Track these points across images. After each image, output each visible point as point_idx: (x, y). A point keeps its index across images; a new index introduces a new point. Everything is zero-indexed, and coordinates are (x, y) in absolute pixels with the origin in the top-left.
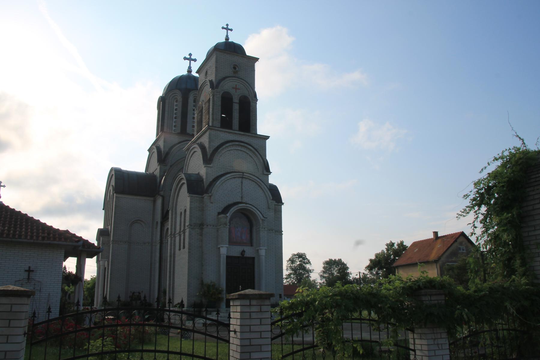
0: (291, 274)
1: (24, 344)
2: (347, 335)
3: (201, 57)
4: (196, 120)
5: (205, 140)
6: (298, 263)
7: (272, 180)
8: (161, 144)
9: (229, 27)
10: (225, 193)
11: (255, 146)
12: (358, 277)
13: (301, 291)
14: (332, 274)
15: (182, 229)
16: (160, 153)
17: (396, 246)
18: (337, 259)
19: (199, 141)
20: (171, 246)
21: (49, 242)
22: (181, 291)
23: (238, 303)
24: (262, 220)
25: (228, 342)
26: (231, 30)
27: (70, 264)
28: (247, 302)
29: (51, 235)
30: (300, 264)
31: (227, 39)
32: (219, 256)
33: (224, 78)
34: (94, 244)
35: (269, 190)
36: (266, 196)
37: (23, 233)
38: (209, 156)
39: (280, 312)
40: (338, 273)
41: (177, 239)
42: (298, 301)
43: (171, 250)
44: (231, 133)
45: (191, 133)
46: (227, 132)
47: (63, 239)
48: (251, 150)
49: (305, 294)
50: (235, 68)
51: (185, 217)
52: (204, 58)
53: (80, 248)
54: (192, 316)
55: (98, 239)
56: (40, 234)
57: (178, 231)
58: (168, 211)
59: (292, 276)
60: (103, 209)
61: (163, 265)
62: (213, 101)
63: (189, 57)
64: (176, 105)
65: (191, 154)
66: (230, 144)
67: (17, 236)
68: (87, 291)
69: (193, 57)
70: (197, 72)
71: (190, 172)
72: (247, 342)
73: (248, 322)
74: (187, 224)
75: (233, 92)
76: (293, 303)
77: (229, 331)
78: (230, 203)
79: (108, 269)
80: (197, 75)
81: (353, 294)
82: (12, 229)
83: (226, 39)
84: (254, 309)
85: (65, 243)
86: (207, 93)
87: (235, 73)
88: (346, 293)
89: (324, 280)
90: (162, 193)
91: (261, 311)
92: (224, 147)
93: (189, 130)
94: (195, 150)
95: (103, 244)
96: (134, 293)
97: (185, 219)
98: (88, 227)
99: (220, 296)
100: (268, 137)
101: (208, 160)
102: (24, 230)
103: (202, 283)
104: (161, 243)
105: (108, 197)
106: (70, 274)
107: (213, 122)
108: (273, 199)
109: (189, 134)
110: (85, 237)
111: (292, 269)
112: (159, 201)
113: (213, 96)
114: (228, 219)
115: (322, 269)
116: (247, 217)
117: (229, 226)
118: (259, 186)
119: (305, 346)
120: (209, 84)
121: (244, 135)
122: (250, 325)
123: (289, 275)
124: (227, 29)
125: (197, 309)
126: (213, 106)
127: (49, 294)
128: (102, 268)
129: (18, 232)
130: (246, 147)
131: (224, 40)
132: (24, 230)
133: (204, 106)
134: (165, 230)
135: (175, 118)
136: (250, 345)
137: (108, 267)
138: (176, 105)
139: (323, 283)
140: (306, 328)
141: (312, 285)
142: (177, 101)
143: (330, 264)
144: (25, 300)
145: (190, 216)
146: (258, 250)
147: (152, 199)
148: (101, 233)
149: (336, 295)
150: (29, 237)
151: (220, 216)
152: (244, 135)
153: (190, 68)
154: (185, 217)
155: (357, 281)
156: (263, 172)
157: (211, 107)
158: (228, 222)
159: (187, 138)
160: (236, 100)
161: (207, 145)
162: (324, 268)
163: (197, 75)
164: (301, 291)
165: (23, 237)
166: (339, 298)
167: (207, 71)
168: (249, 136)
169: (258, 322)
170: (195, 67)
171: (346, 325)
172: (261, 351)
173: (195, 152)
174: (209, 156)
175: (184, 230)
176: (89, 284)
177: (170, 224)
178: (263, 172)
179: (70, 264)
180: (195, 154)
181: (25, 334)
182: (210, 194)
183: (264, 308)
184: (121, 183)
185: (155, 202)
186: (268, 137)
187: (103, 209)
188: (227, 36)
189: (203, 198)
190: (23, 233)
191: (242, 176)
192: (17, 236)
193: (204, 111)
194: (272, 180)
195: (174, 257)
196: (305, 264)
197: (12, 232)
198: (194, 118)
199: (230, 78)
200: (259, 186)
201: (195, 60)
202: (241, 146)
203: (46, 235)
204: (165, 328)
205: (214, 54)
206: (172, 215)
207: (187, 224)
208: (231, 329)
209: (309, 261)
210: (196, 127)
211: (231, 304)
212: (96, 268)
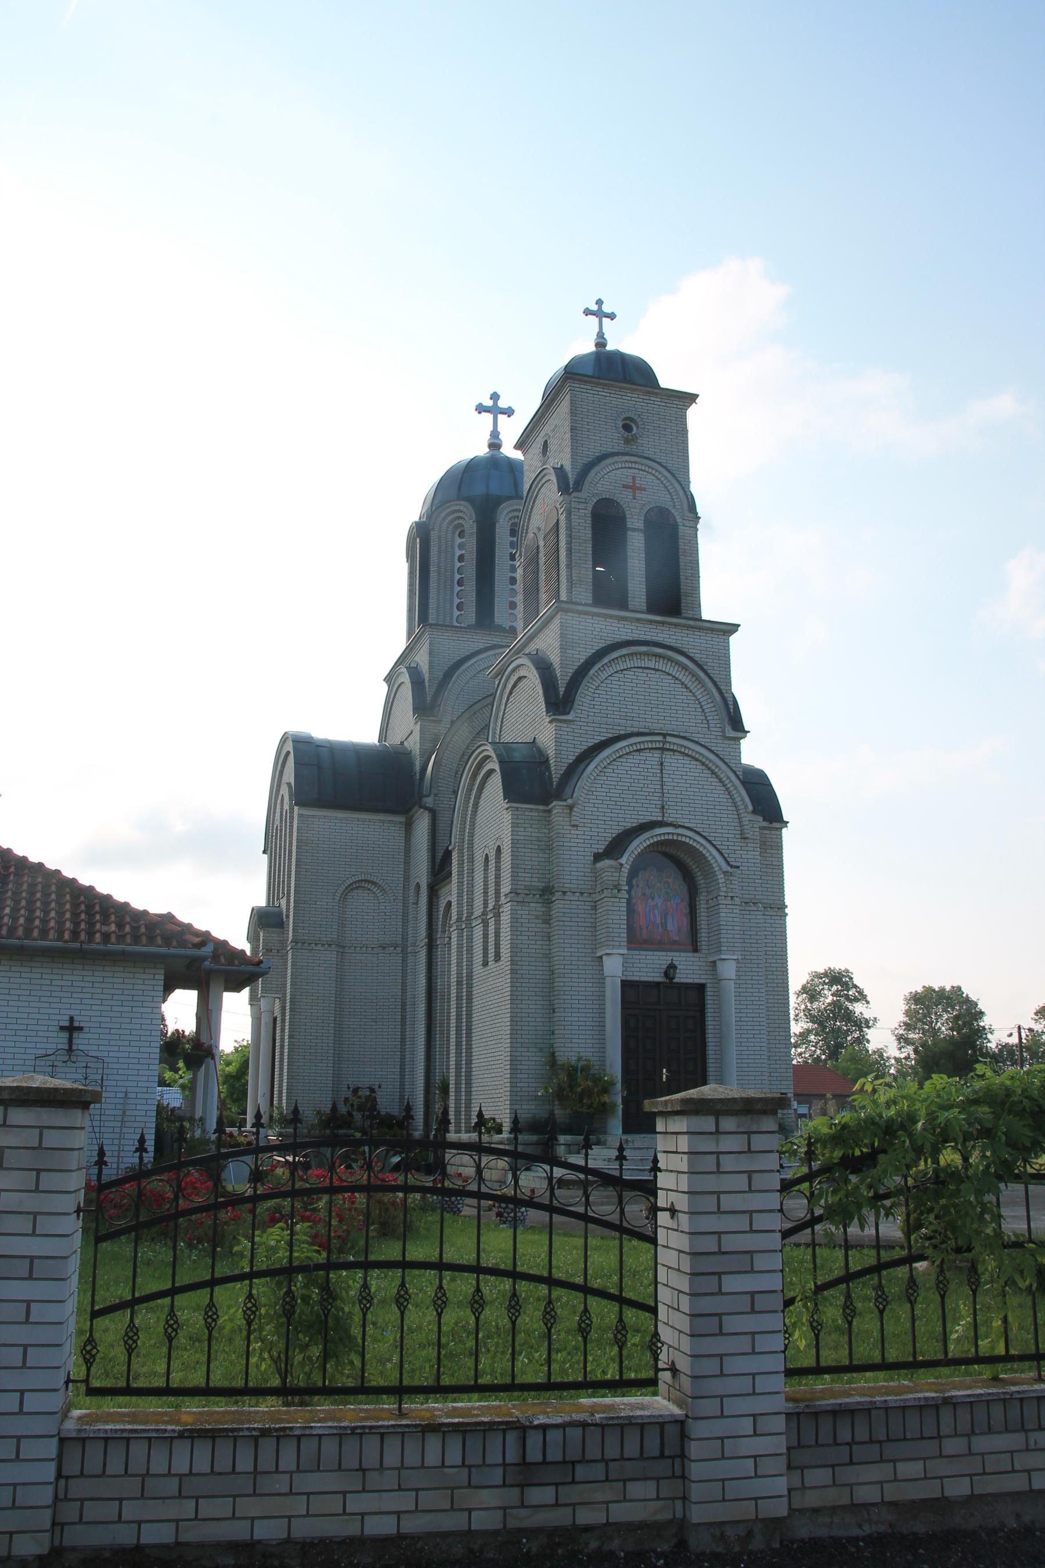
0: (808, 1032)
1: (78, 1236)
2: (1013, 1224)
3: (526, 403)
4: (519, 587)
5: (549, 643)
6: (830, 999)
7: (752, 753)
8: (422, 658)
9: (606, 309)
10: (607, 800)
11: (695, 653)
12: (1014, 1040)
13: (869, 1088)
14: (935, 1032)
15: (491, 905)
16: (419, 684)
18: (948, 988)
19: (531, 648)
20: (460, 953)
21: (121, 947)
22: (493, 1085)
23: (680, 1124)
24: (725, 873)
25: (653, 1241)
26: (612, 316)
27: (180, 1011)
28: (707, 1123)
29: (128, 929)
30: (833, 1003)
31: (601, 343)
33: (600, 459)
34: (243, 952)
35: (744, 783)
36: (734, 803)
37: (52, 924)
39: (806, 1153)
40: (951, 1029)
41: (478, 932)
42: (859, 1119)
43: (459, 965)
44: (625, 619)
45: (507, 625)
46: (612, 617)
47: (159, 940)
48: (685, 668)
49: (882, 1099)
50: (627, 428)
51: (498, 869)
52: (536, 403)
53: (204, 965)
54: (519, 1159)
55: (252, 937)
56: (98, 926)
57: (478, 911)
58: (448, 854)
59: (812, 1037)
60: (264, 852)
61: (437, 1013)
62: (569, 528)
63: (490, 403)
64: (461, 546)
65: (509, 686)
66: (624, 651)
67: (36, 933)
68: (224, 1083)
69: (502, 404)
70: (520, 445)
71: (507, 738)
72: (709, 1244)
73: (711, 1183)
74: (505, 889)
75: (624, 498)
76: (844, 1127)
77: (654, 1209)
78: (629, 825)
79: (283, 1021)
80: (518, 455)
81: (1030, 1098)
82: (22, 912)
83: (597, 345)
84: (728, 1143)
85: (164, 950)
86: (547, 505)
87: (627, 441)
88: (1008, 1095)
89: (909, 1050)
90: (429, 801)
91: (750, 1151)
92: (606, 660)
93: (500, 617)
94: (522, 672)
95: (268, 950)
96: (356, 1090)
97: (498, 877)
98: (223, 904)
99: (606, 1099)
100: (733, 628)
101: (559, 701)
102: (53, 914)
103: (552, 1062)
104: (431, 946)
105: (277, 817)
106: (178, 1035)
107: (570, 591)
108: (754, 812)
109: (500, 629)
110: (219, 934)
111: (812, 1018)
112: (422, 824)
113: (569, 513)
114: (625, 870)
115: (903, 1018)
116: (680, 862)
117: (629, 892)
118: (713, 773)
119: (886, 1256)
120: (554, 478)
121: (663, 623)
122: (719, 1193)
123: (804, 1035)
124: (599, 313)
125: (536, 1139)
126: (569, 543)
127: (126, 1093)
128: (265, 1019)
129: (37, 922)
130: (670, 659)
131: (592, 348)
132: (53, 914)
133: (541, 543)
134: (442, 909)
135: (460, 583)
136: (721, 1253)
137: (283, 1014)
138: (461, 546)
139: (907, 1058)
140: (887, 1203)
141: (875, 1065)
142: (461, 535)
143: (926, 1003)
144: (77, 1117)
145: (515, 867)
146: (714, 962)
147: (401, 819)
148: (264, 921)
149: (976, 1102)
150: (67, 936)
151: (600, 865)
152: (663, 623)
153: (495, 434)
154: (498, 869)
155: (1007, 1054)
157: (563, 544)
158: (624, 880)
159: (496, 641)
160: (635, 521)
161: (555, 658)
162: (907, 1013)
163: (518, 455)
164: (869, 1088)
165: (52, 934)
166: (987, 1109)
167: (546, 442)
168: (676, 625)
169: (742, 1183)
170: (511, 431)
171: (1011, 1191)
172: (752, 1271)
173: (520, 679)
174: (562, 690)
175: (497, 907)
176: (228, 1064)
177: (455, 891)
178: (723, 731)
179: (180, 1011)
180: (521, 685)
181: (78, 1211)
182: (570, 801)
183: (759, 1142)
184: (318, 780)
185: (409, 826)
186: (733, 628)
187: (264, 852)
188: (601, 335)
189: (550, 811)
190: (52, 924)
191: (664, 742)
192: (36, 933)
193: (542, 559)
194: (752, 753)
195: (470, 986)
196: (851, 1001)
197: (22, 921)
198: (513, 581)
199: (616, 459)
200: (713, 773)
201: (509, 412)
202: (656, 655)
203: (113, 927)
204: (450, 1196)
205: (566, 389)
206: (461, 863)
207: (505, 889)
208: (661, 1202)
209: (861, 992)
210: (520, 607)
211: (660, 1126)
212: (248, 1020)
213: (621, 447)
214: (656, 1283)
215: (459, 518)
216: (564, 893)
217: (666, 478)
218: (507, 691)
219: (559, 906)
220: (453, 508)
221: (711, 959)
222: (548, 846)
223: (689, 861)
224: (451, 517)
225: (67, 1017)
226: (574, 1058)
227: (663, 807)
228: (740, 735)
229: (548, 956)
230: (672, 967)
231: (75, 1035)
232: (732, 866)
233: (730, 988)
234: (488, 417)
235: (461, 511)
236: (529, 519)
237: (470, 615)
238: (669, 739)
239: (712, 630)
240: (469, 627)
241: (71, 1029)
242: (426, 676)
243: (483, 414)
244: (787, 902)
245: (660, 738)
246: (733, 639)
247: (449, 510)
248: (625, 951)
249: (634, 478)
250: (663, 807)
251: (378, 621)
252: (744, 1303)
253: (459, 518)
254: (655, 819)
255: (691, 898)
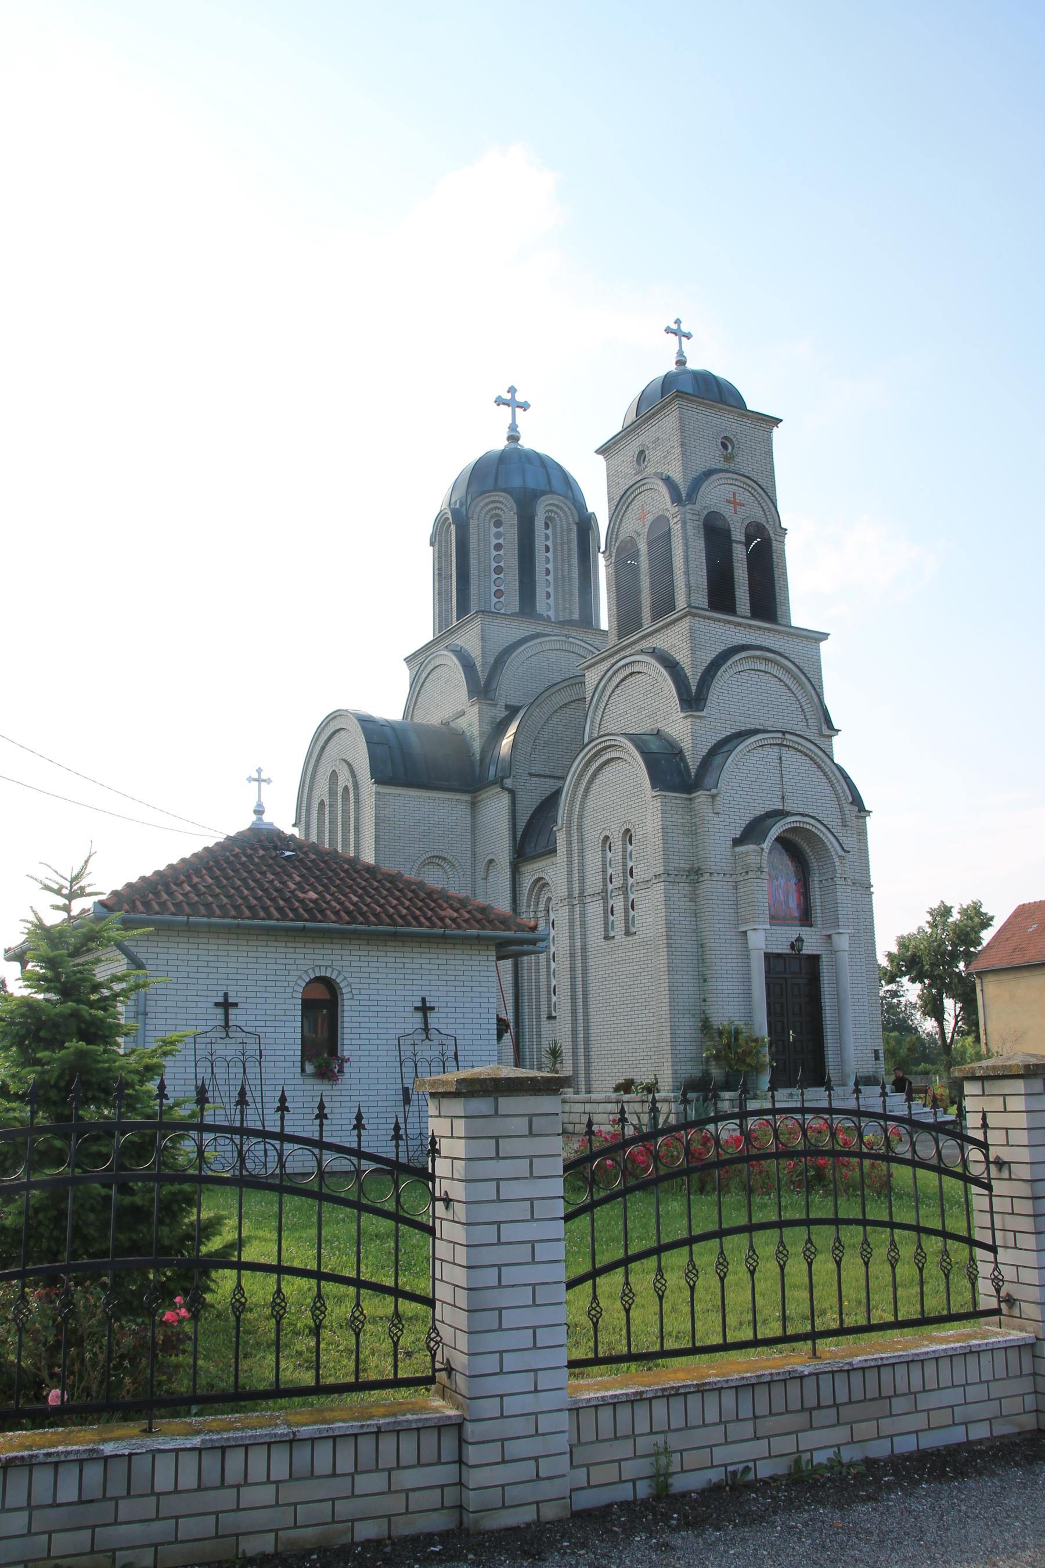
10: (747, 784)
17: (955, 916)
32: (746, 952)
38: (694, 688)
50: (725, 446)
64: (498, 535)
75: (727, 511)
78: (758, 813)
100: (825, 636)
101: (692, 699)
103: (706, 1026)
118: (819, 767)
130: (777, 663)
135: (498, 570)
142: (498, 524)
146: (829, 936)
147: (467, 797)
156: (820, 730)
159: (540, 629)
160: (738, 534)
174: (694, 688)
178: (820, 730)
182: (714, 791)
186: (825, 636)
195: (584, 958)
199: (721, 475)
200: (819, 767)
213: (721, 465)
214: (434, 1279)
215: (496, 508)
216: (711, 874)
217: (760, 495)
218: (614, 683)
219: (709, 886)
220: (492, 499)
221: (825, 933)
222: (693, 832)
223: (805, 846)
224: (489, 507)
225: (221, 994)
226: (725, 1023)
227: (783, 797)
228: (833, 733)
229: (697, 931)
230: (800, 940)
231: (231, 1011)
232: (845, 851)
233: (845, 958)
234: (507, 410)
235: (500, 502)
236: (621, 522)
237: (512, 601)
238: (788, 736)
239: (807, 638)
240: (513, 614)
241: (226, 1005)
242: (478, 665)
243: (502, 406)
244: (872, 882)
245: (780, 735)
246: (823, 645)
247: (488, 500)
248: (768, 927)
249: (734, 494)
250: (783, 797)
251: (407, 605)
252: (525, 1296)
253: (496, 508)
254: (776, 807)
255: (805, 878)
